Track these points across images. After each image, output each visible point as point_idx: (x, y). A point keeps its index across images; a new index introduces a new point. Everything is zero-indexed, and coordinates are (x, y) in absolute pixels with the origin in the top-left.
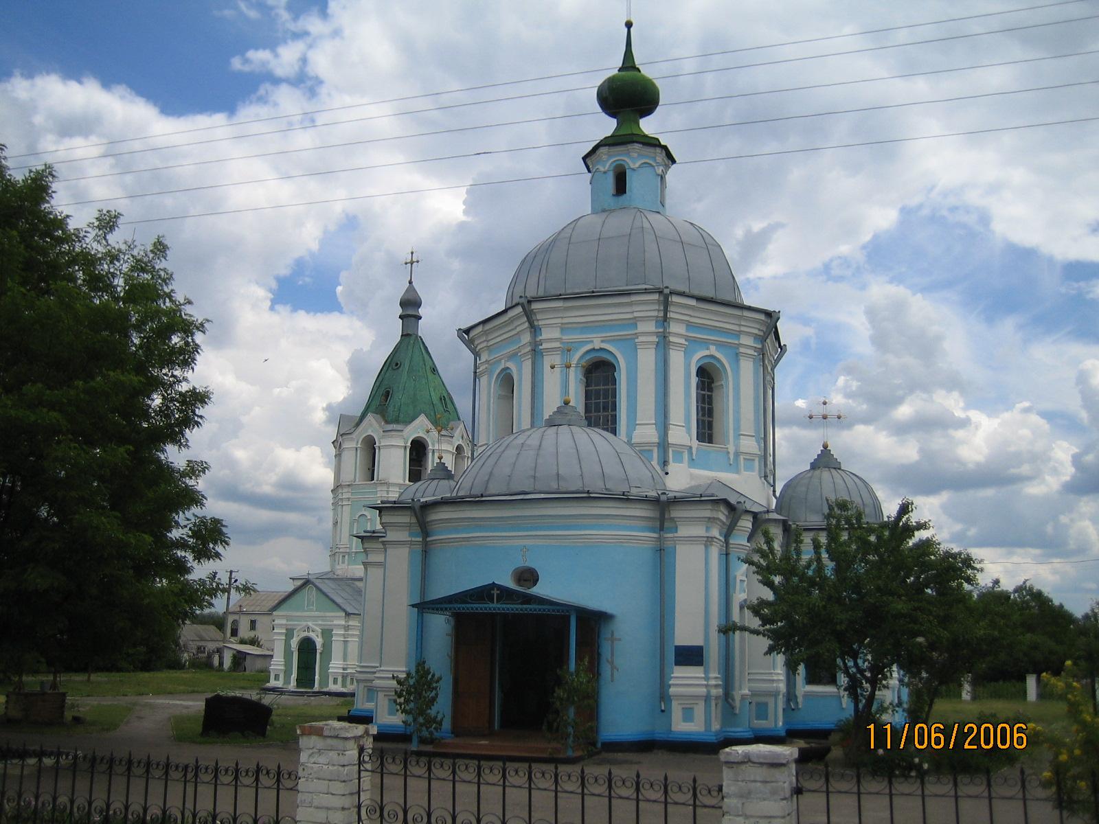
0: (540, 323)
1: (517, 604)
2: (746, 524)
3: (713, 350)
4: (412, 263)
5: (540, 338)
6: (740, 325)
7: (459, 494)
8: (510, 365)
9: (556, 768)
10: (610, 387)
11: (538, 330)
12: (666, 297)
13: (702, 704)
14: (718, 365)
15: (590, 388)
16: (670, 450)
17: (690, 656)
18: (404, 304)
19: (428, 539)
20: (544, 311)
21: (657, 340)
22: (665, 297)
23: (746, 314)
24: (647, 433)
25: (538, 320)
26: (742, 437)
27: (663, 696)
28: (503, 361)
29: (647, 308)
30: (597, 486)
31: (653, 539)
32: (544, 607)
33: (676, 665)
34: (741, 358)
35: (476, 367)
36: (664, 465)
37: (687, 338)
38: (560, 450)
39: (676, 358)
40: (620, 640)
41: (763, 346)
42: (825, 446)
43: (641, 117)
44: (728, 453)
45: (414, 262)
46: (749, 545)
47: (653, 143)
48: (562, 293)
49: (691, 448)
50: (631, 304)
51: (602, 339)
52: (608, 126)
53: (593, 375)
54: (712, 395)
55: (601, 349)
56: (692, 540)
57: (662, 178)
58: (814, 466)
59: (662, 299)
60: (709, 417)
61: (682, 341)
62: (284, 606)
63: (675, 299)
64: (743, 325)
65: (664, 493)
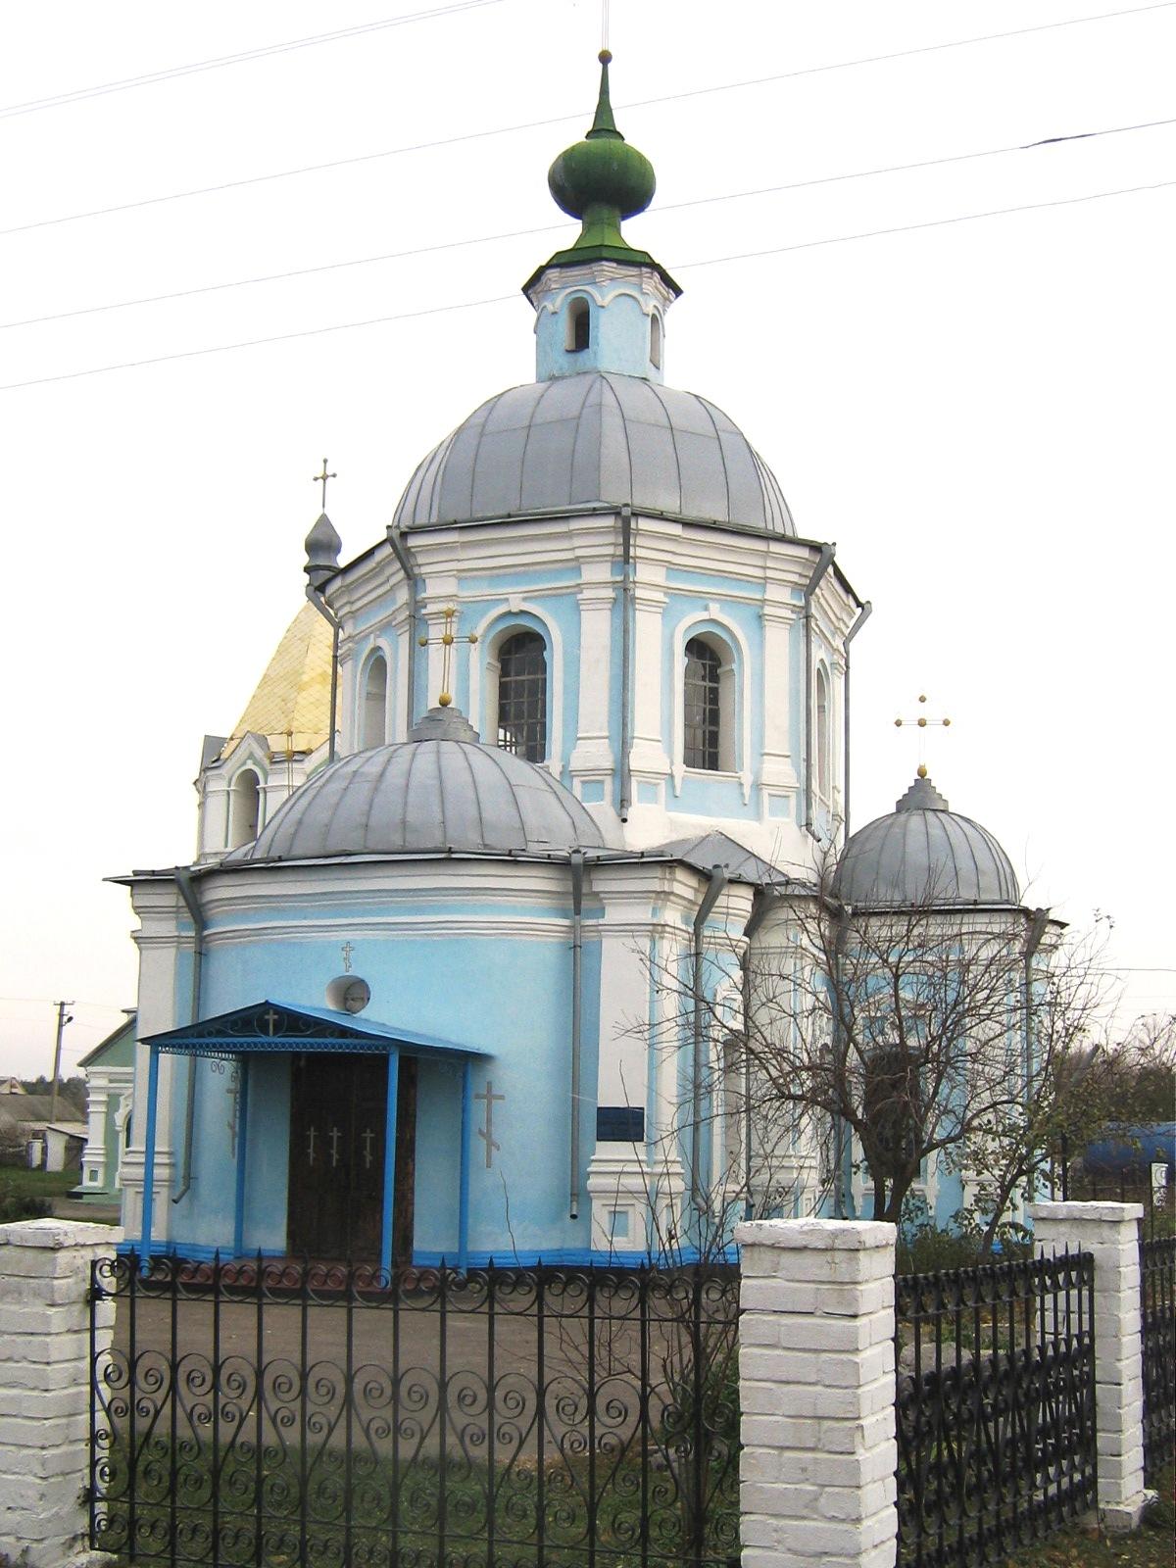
0: (424, 570)
2: (740, 902)
3: (716, 611)
4: (325, 478)
5: (424, 595)
6: (765, 568)
7: (254, 857)
8: (382, 642)
10: (539, 676)
11: (420, 583)
12: (626, 522)
13: (641, 1208)
14: (724, 636)
15: (508, 679)
16: (634, 780)
17: (623, 1124)
18: (312, 547)
19: (206, 933)
20: (429, 549)
21: (613, 595)
22: (625, 519)
23: (775, 547)
24: (595, 754)
25: (420, 566)
26: (765, 757)
27: (576, 1196)
28: (372, 636)
29: (594, 540)
30: (468, 839)
31: (563, 929)
32: (347, 1041)
33: (598, 1140)
34: (766, 623)
35: (336, 647)
36: (622, 806)
37: (668, 591)
38: (414, 782)
39: (648, 628)
40: (502, 1097)
41: (808, 602)
42: (922, 773)
43: (624, 218)
44: (741, 785)
45: (328, 476)
46: (746, 939)
47: (641, 262)
48: (459, 518)
49: (672, 776)
50: (568, 535)
51: (525, 595)
52: (568, 231)
53: (513, 657)
54: (717, 689)
55: (523, 612)
56: (628, 929)
57: (655, 320)
58: (902, 806)
59: (620, 524)
61: (659, 596)
62: (107, 1055)
63: (644, 524)
64: (769, 568)
65: (577, 851)
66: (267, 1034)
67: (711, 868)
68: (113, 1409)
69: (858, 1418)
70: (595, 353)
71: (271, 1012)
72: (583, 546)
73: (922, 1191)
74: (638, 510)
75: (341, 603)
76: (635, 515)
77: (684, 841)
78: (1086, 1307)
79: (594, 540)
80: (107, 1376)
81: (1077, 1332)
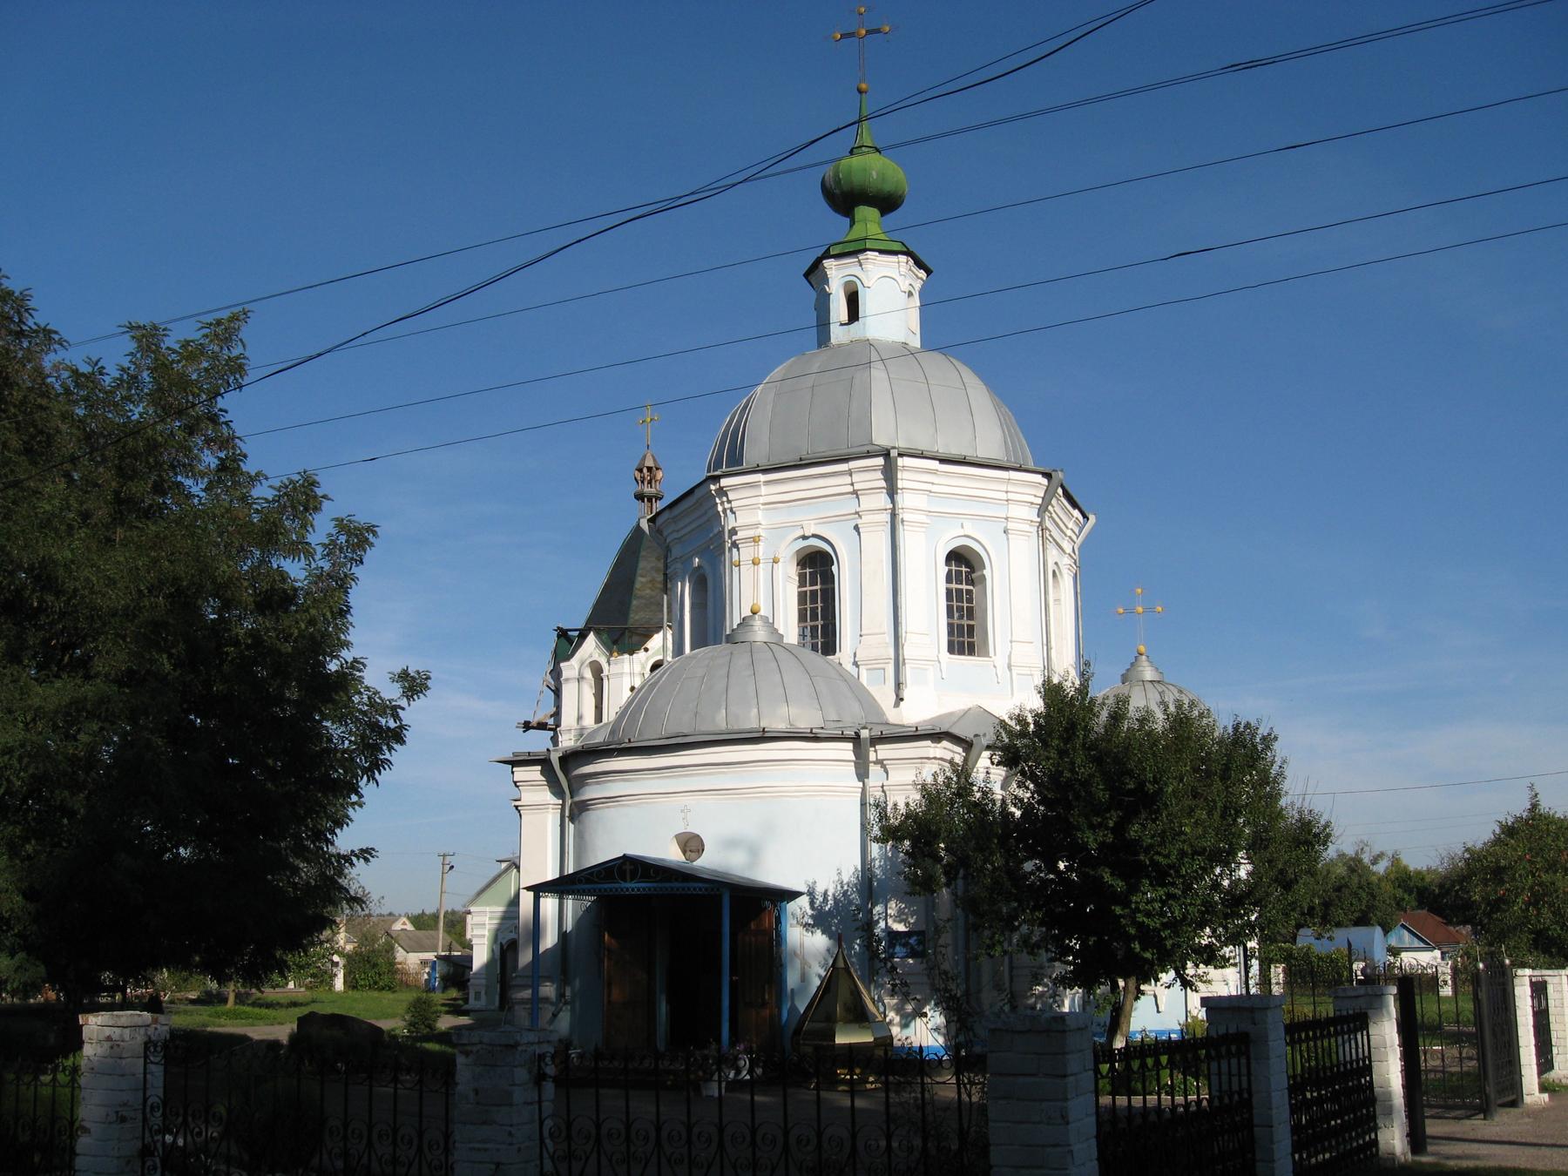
1: (656, 882)
9: (1091, 1070)
20: (735, 488)
29: (868, 474)
60: (969, 619)
66: (625, 881)
67: (972, 737)
68: (556, 1156)
69: (1069, 1145)
70: (864, 324)
71: (628, 863)
74: (902, 451)
75: (670, 531)
76: (901, 455)
77: (951, 714)
78: (1244, 1070)
79: (868, 474)
80: (551, 1135)
81: (1237, 1089)
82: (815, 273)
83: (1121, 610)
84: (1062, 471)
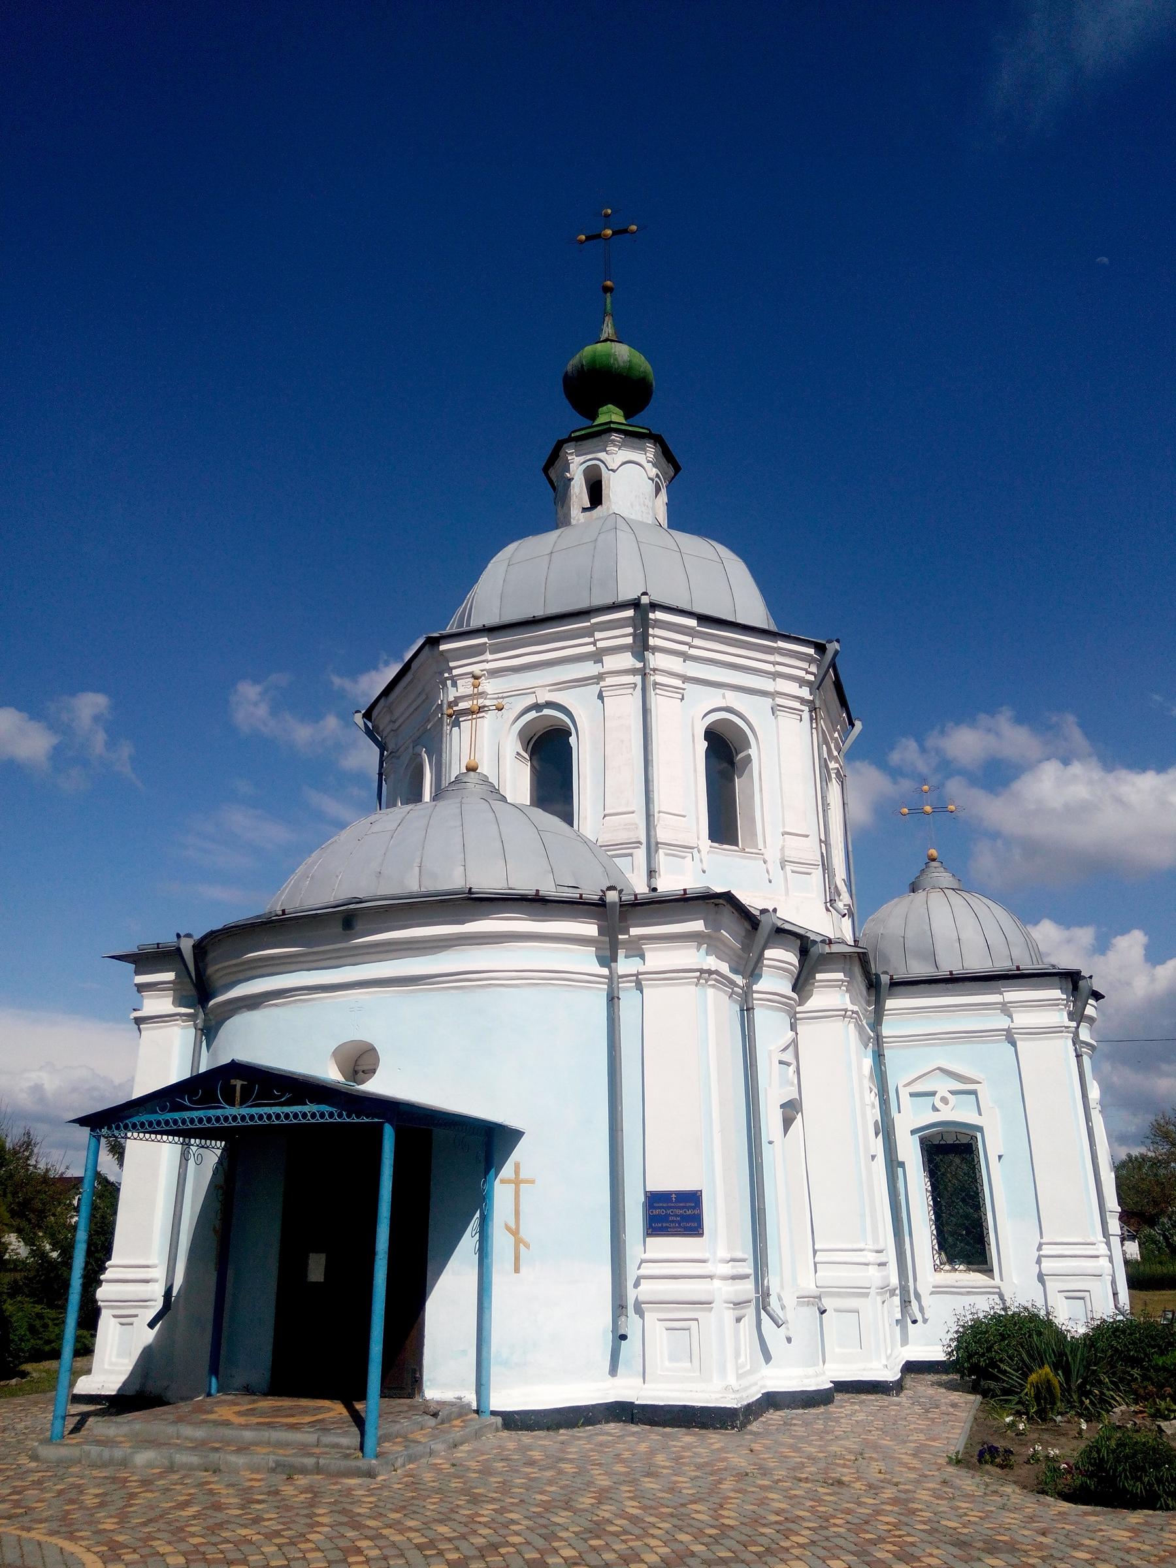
3: (733, 699)
65: (645, 594)
66: (232, 1104)
72: (605, 638)
73: (999, 1288)
82: (555, 457)
83: (905, 810)
84: (838, 641)
